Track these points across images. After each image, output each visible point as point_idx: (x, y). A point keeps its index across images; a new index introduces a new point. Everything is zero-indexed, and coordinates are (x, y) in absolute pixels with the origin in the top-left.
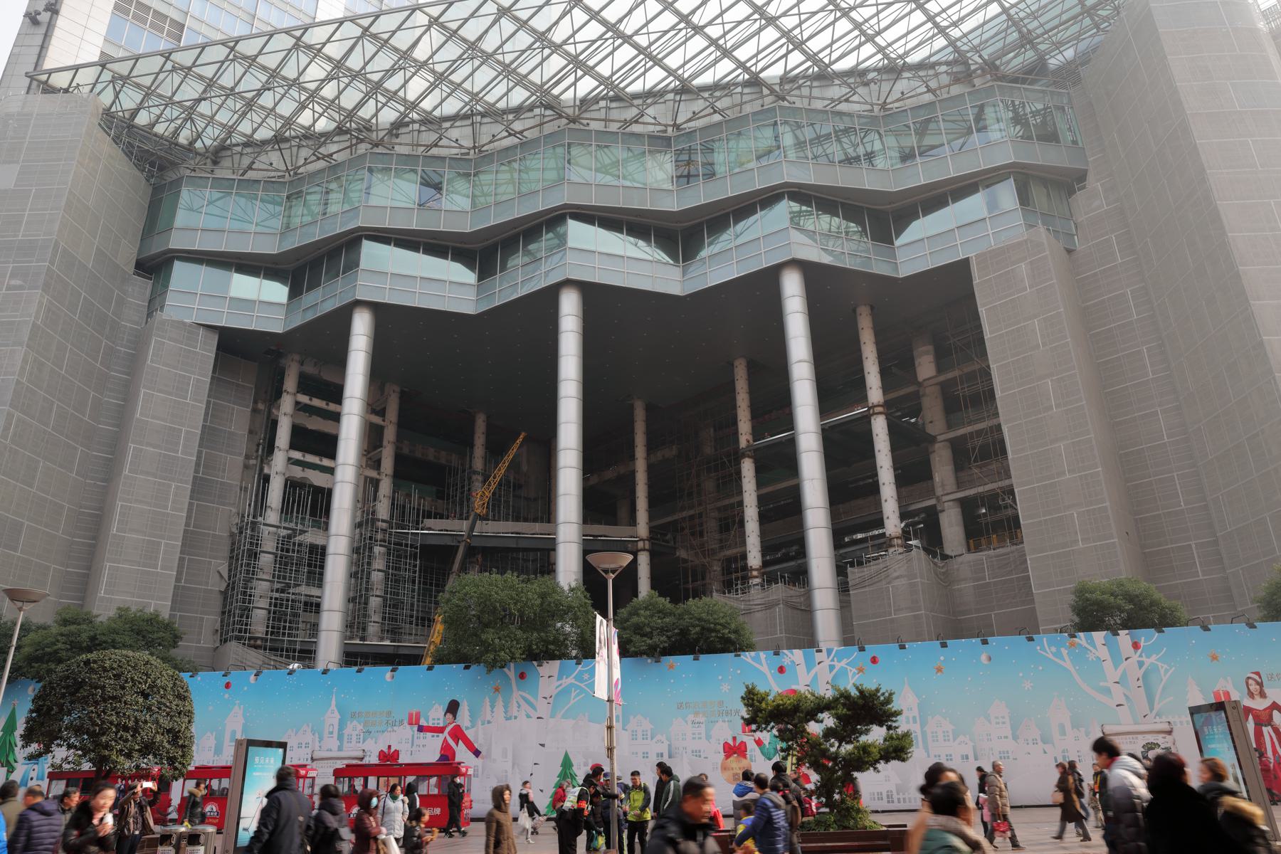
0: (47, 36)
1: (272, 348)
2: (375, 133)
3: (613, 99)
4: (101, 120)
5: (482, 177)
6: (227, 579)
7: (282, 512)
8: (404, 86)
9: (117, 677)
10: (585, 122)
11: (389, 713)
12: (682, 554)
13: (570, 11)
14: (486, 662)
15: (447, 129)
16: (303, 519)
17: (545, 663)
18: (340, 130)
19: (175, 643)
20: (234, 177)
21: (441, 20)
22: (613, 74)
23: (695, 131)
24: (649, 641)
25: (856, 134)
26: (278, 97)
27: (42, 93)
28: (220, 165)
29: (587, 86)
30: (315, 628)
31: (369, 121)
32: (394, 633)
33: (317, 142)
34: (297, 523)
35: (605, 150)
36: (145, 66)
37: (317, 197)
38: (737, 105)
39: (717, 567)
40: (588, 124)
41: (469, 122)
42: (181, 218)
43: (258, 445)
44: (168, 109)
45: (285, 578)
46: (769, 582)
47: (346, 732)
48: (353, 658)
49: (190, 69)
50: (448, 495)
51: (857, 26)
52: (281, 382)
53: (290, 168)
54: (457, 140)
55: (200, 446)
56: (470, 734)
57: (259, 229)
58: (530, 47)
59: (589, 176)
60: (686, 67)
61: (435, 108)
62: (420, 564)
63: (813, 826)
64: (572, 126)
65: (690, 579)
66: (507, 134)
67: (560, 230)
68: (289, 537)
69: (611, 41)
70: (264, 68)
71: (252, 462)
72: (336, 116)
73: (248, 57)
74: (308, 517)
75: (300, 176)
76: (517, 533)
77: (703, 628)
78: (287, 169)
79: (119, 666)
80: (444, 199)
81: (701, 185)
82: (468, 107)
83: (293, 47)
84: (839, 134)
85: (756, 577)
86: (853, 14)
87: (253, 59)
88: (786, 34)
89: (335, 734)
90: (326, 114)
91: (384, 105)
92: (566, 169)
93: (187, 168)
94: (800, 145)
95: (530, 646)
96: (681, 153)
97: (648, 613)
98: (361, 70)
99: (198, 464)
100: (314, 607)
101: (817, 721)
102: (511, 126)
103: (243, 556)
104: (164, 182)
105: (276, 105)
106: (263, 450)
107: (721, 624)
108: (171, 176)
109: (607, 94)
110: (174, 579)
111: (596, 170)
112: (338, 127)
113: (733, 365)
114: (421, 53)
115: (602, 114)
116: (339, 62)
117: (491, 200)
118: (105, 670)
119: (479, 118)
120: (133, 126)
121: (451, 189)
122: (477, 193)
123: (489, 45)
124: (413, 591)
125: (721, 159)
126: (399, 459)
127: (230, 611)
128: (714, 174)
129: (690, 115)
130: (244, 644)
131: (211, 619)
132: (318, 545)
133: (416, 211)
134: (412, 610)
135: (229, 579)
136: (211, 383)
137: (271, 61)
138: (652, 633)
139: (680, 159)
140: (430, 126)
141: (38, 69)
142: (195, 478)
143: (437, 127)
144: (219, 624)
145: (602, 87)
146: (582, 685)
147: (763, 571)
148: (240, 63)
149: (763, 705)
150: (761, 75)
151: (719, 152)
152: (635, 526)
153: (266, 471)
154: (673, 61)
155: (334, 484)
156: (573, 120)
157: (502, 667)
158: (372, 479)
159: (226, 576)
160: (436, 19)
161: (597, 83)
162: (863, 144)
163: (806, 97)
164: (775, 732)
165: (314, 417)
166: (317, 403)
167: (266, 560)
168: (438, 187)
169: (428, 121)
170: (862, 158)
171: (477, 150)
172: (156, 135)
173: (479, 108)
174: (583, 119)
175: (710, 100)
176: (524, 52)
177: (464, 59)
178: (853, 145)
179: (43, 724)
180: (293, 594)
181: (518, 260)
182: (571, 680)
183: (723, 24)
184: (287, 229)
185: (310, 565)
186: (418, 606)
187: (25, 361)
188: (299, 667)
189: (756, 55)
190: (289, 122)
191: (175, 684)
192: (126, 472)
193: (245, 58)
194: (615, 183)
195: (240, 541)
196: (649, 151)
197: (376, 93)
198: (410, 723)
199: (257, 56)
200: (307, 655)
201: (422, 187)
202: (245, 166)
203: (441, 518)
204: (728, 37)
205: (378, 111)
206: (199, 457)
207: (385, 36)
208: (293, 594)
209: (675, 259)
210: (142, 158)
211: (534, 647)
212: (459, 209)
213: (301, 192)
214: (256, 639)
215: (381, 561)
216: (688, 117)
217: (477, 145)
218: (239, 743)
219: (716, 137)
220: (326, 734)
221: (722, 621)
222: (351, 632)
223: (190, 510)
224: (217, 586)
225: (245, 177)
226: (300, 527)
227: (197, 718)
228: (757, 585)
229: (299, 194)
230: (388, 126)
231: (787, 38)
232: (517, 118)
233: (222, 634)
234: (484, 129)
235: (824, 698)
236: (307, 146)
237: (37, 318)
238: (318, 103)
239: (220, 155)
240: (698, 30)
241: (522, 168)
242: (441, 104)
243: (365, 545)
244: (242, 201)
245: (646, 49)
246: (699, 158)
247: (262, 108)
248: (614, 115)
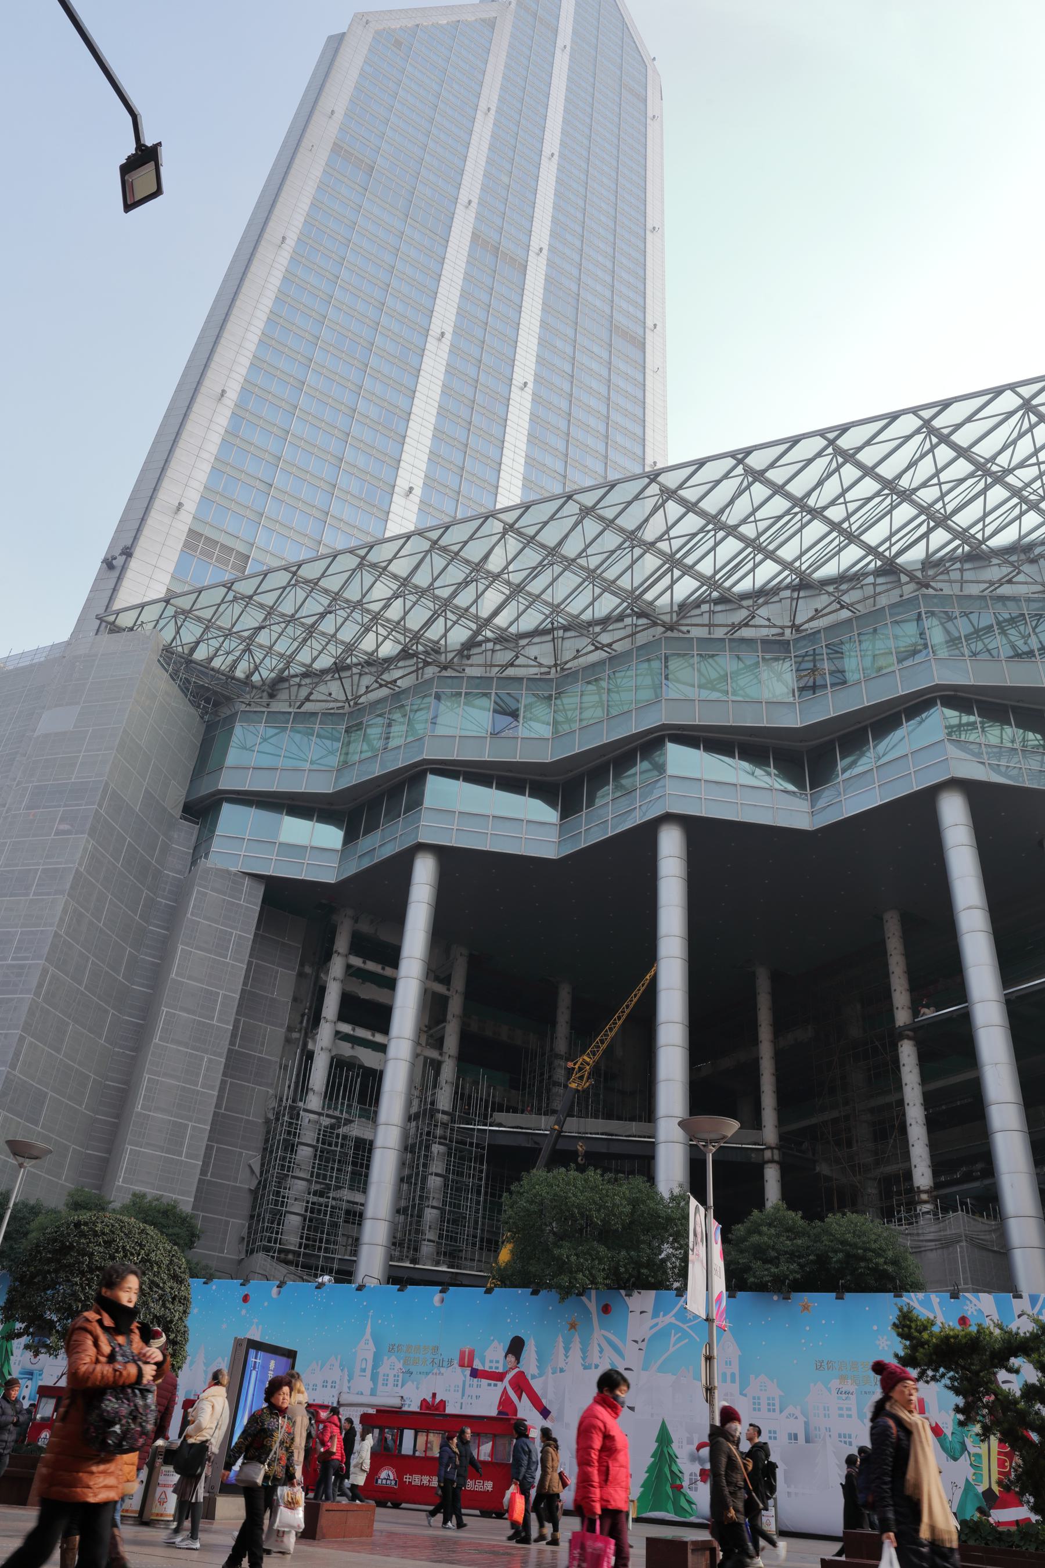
0: (119, 579)
1: (324, 901)
2: (443, 655)
3: (717, 602)
4: (161, 656)
5: (566, 701)
6: (258, 1175)
7: (325, 1097)
8: (476, 601)
9: (108, 1244)
10: (684, 629)
11: (436, 1349)
12: (823, 1169)
13: (663, 505)
14: (559, 1287)
15: (524, 647)
16: (350, 1106)
17: (635, 1293)
18: (405, 654)
19: (193, 1243)
20: (290, 710)
21: (516, 526)
22: (716, 573)
23: (819, 632)
24: (774, 1270)
25: (1026, 623)
26: (340, 620)
27: (109, 633)
28: (278, 697)
29: (686, 587)
30: (355, 1243)
31: (438, 642)
32: (452, 1256)
33: (380, 669)
34: (342, 1112)
35: (710, 660)
36: (205, 599)
37: (379, 730)
38: (869, 598)
39: (872, 1190)
40: (688, 632)
41: (549, 637)
42: (233, 756)
43: (303, 1015)
44: (227, 641)
45: (325, 1177)
46: (945, 1210)
47: (383, 1370)
48: (398, 1278)
49: (251, 597)
50: (524, 1084)
51: (1015, 492)
52: (332, 941)
53: (349, 698)
54: (536, 658)
55: (238, 1013)
56: (536, 1385)
57: (315, 767)
58: (619, 547)
59: (692, 693)
60: (804, 559)
61: (511, 624)
62: (488, 1170)
63: (1016, 1539)
64: (669, 634)
65: (836, 1205)
66: (593, 648)
67: (657, 756)
68: (333, 1127)
69: (712, 533)
70: (326, 591)
71: (295, 1035)
72: (401, 638)
73: (310, 581)
74: (355, 1104)
75: (360, 706)
76: (606, 1134)
77: (848, 1255)
78: (347, 699)
79: (111, 1231)
80: (521, 726)
81: (830, 694)
82: (549, 620)
83: (358, 565)
84: (1002, 626)
85: (925, 1202)
86: (1010, 479)
87: (316, 582)
88: (924, 510)
89: (369, 1372)
90: (390, 637)
91: (455, 623)
92: (664, 686)
93: (242, 702)
94: (953, 641)
95: (616, 1269)
96: (803, 661)
97: (773, 1231)
98: (429, 586)
99: (234, 1035)
100: (356, 1216)
101: (1011, 1370)
102: (598, 639)
103: (278, 1148)
104: (218, 718)
105: (337, 630)
106: (308, 1021)
107: (873, 1251)
108: (225, 712)
109: (710, 595)
110: (198, 1171)
111: (700, 687)
112: (403, 650)
113: (882, 919)
114: (495, 564)
115: (705, 619)
116: (405, 579)
117: (576, 726)
118: (96, 1234)
119: (561, 633)
120: (191, 661)
121: (529, 716)
122: (560, 719)
123: (570, 550)
124: (478, 1203)
125: (852, 664)
126: (465, 1038)
127: (259, 1215)
128: (845, 682)
129: (811, 613)
130: (273, 1257)
131: (237, 1224)
132: (366, 1140)
133: (488, 739)
134: (476, 1228)
135: (261, 1176)
136: (254, 941)
137: (333, 583)
138: (777, 1258)
139: (801, 668)
140: (506, 645)
141: (108, 610)
142: (230, 1051)
143: (514, 645)
144: (246, 1230)
145: (705, 587)
146: (685, 1327)
147: (935, 1193)
148: (301, 588)
149: (925, 1335)
150: (899, 561)
151: (850, 657)
152: (761, 1129)
153: (310, 1046)
154: (788, 553)
155: (386, 1062)
156: (671, 628)
157: (580, 1294)
158: (433, 1061)
159: (257, 1171)
160: (512, 526)
161: (699, 583)
162: (1036, 634)
163: (955, 582)
164: (946, 1381)
165: (368, 984)
166: (372, 966)
167: (304, 1153)
168: (514, 714)
169: (504, 639)
170: (1037, 653)
171: (558, 668)
172: (213, 669)
173: (560, 620)
174: (682, 625)
175: (836, 594)
176: (613, 552)
177: (545, 566)
178: (1023, 637)
179: (25, 1294)
180: (334, 1199)
181: (606, 795)
182: (669, 1319)
183: (845, 503)
184: (345, 766)
185: (354, 1164)
186: (483, 1224)
187: (65, 911)
188: (330, 1281)
189: (889, 538)
190: (350, 648)
191: (171, 1261)
192: (156, 1040)
193: (307, 582)
194: (725, 698)
195: (275, 1129)
196: (764, 659)
197: (445, 611)
198: (462, 1365)
199: (319, 579)
200: (345, 1275)
201: (496, 715)
202: (302, 698)
203: (515, 1111)
204: (852, 520)
205: (447, 631)
206: (236, 1027)
207: (456, 548)
208: (334, 1199)
209: (801, 786)
210: (197, 694)
211: (622, 1270)
212: (537, 737)
213: (361, 723)
214: (288, 1251)
215: (440, 1163)
216: (810, 616)
217: (559, 662)
218: (238, 1343)
219: (843, 638)
221: (874, 1246)
222: (400, 1252)
223: (222, 1090)
224: (246, 1182)
225: (302, 710)
226: (345, 1115)
227: (194, 1310)
228: (928, 1213)
229: (359, 726)
230: (458, 647)
231: (927, 515)
232: (604, 630)
233: (248, 1242)
234: (567, 644)
235: (1017, 1334)
236: (370, 674)
237: (80, 864)
238: (383, 626)
239: (277, 687)
240: (817, 513)
241: (611, 687)
242: (517, 619)
243: (421, 1142)
244: (297, 737)
245: (754, 541)
246: (826, 666)
247: (323, 634)
248: (719, 619)
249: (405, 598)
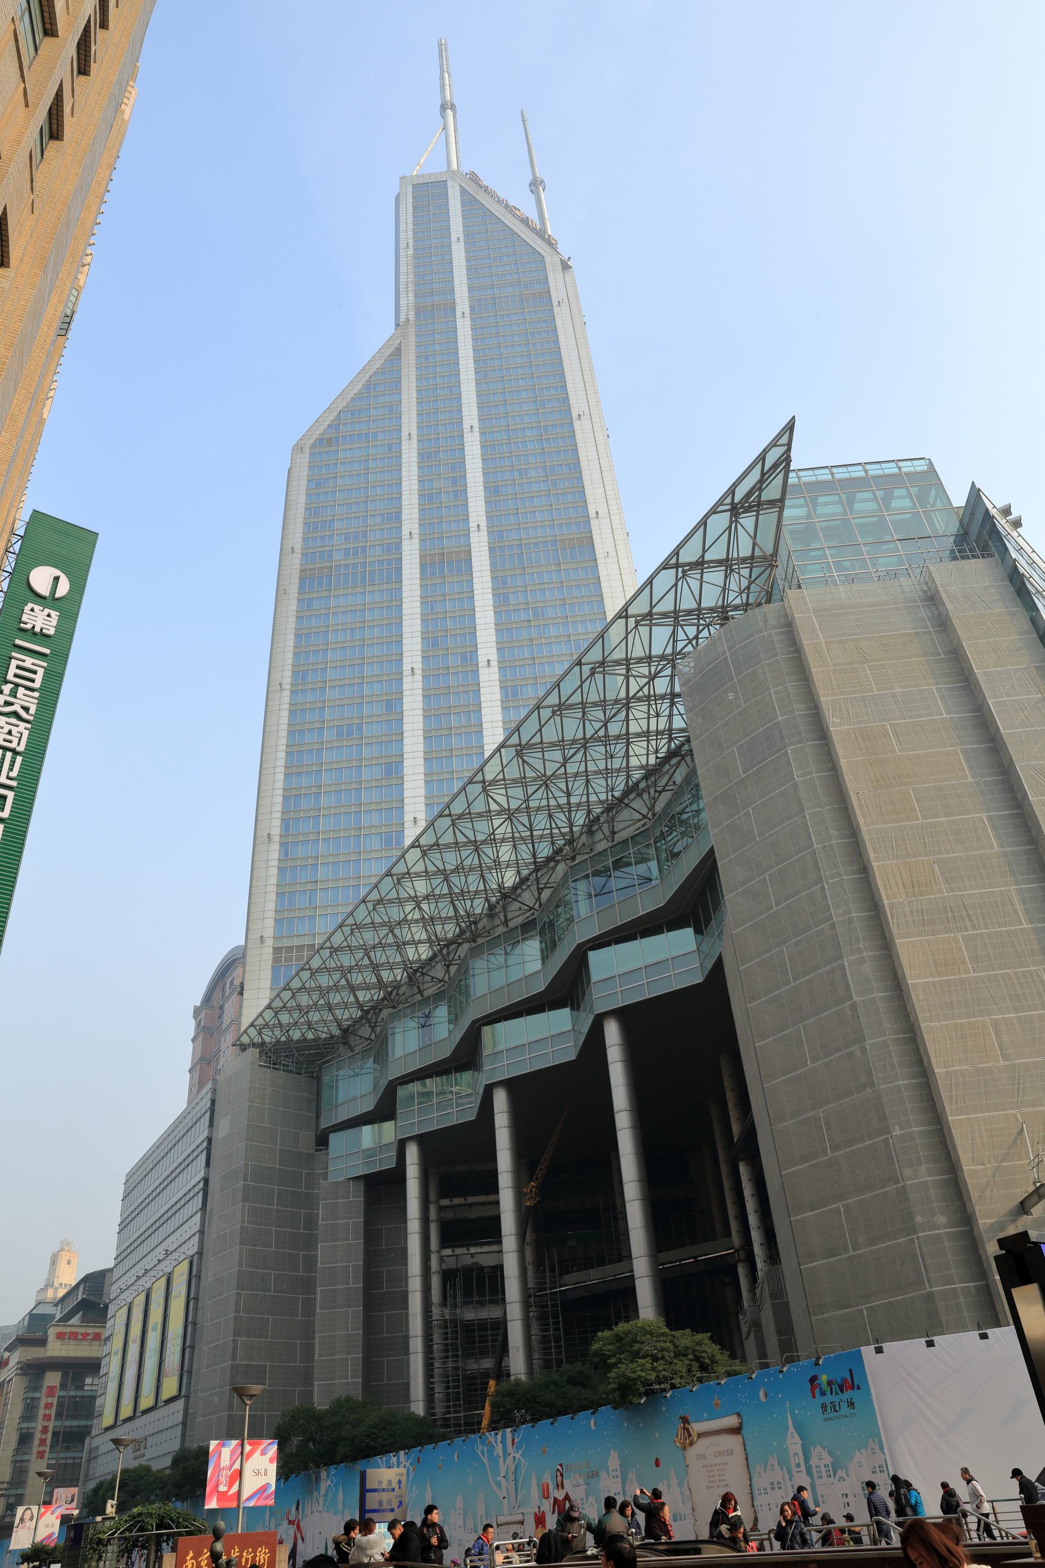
36: (569, 686)
220: (794, 1469)
249: (688, 639)
